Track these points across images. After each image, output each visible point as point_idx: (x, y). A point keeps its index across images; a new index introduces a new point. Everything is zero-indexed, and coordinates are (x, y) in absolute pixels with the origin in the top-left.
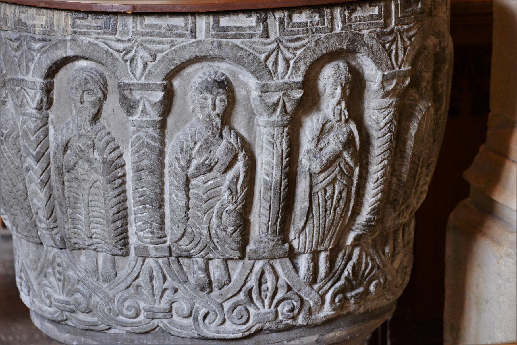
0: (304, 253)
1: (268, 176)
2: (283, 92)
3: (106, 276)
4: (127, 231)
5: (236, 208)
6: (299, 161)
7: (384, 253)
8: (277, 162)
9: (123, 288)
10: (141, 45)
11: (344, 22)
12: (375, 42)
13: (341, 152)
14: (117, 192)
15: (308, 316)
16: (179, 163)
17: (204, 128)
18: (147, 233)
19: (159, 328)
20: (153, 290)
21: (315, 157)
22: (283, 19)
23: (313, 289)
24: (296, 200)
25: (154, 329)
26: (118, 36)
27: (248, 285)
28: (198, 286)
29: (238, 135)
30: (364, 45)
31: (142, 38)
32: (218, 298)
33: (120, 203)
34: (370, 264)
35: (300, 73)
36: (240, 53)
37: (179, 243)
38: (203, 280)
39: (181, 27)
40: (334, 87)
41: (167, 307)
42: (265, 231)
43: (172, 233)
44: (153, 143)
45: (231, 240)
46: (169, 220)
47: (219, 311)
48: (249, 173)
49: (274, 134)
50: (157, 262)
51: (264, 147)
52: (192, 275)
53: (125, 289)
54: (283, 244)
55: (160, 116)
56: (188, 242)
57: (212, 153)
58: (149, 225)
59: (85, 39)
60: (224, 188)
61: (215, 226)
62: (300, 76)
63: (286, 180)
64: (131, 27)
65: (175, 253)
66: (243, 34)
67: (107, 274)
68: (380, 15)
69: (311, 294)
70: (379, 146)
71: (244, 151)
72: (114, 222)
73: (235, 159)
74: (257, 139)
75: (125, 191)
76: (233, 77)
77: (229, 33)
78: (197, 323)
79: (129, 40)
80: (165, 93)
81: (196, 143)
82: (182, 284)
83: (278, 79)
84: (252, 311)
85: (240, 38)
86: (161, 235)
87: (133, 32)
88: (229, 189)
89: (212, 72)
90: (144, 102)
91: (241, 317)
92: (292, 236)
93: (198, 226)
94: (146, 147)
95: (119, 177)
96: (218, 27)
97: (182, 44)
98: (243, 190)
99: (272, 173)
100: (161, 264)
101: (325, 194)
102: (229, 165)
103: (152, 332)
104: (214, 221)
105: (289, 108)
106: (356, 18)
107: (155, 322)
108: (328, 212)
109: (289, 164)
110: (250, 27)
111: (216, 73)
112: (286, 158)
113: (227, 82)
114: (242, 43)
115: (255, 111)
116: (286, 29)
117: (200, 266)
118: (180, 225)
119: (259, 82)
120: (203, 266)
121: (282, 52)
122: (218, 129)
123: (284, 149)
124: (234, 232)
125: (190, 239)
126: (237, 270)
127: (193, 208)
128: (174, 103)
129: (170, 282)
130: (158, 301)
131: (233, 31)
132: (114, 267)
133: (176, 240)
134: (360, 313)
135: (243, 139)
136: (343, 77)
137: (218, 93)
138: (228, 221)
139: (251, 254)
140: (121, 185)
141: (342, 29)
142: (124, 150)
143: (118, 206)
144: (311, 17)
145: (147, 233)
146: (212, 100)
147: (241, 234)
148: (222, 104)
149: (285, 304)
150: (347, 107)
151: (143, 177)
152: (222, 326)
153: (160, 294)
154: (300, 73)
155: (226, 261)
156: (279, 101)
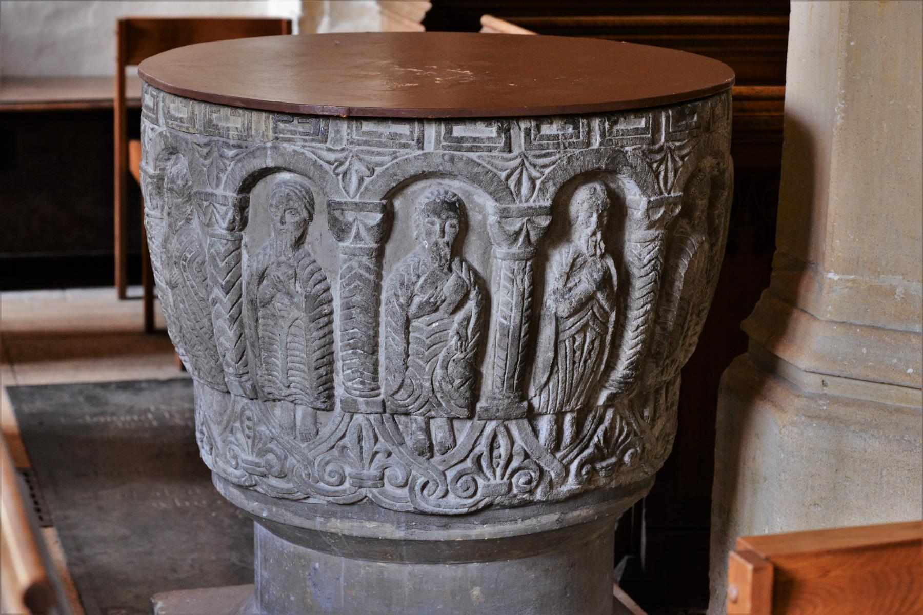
0: (546, 413)
4: (332, 380)
7: (642, 417)
10: (357, 156)
11: (603, 135)
12: (639, 161)
13: (595, 292)
14: (321, 332)
16: (398, 300)
18: (356, 383)
21: (563, 298)
22: (530, 130)
23: (555, 457)
25: (362, 500)
26: (328, 145)
27: (477, 450)
29: (470, 268)
30: (627, 164)
32: (440, 465)
33: (325, 346)
34: (625, 430)
35: (548, 196)
37: (395, 396)
40: (588, 214)
42: (499, 385)
44: (367, 275)
50: (368, 420)
55: (376, 243)
56: (406, 396)
57: (439, 289)
59: (288, 147)
60: (451, 332)
61: (439, 378)
64: (345, 134)
68: (646, 129)
70: (641, 287)
72: (316, 369)
73: (466, 297)
75: (331, 332)
79: (343, 150)
81: (419, 277)
83: (521, 202)
84: (481, 482)
89: (442, 192)
90: (358, 226)
92: (532, 392)
95: (325, 315)
98: (474, 336)
100: (373, 422)
101: (574, 343)
104: (439, 371)
105: (533, 238)
106: (618, 131)
107: (363, 491)
108: (577, 365)
110: (490, 139)
111: (446, 193)
113: (460, 204)
114: (479, 157)
115: (492, 241)
122: (447, 261)
126: (464, 431)
129: (382, 444)
130: (367, 466)
132: (316, 423)
134: (611, 489)
135: (476, 273)
136: (600, 202)
137: (447, 218)
140: (327, 325)
141: (601, 144)
144: (563, 128)
147: (470, 389)
149: (520, 475)
150: (604, 238)
154: (548, 196)
155: (451, 420)
156: (521, 230)
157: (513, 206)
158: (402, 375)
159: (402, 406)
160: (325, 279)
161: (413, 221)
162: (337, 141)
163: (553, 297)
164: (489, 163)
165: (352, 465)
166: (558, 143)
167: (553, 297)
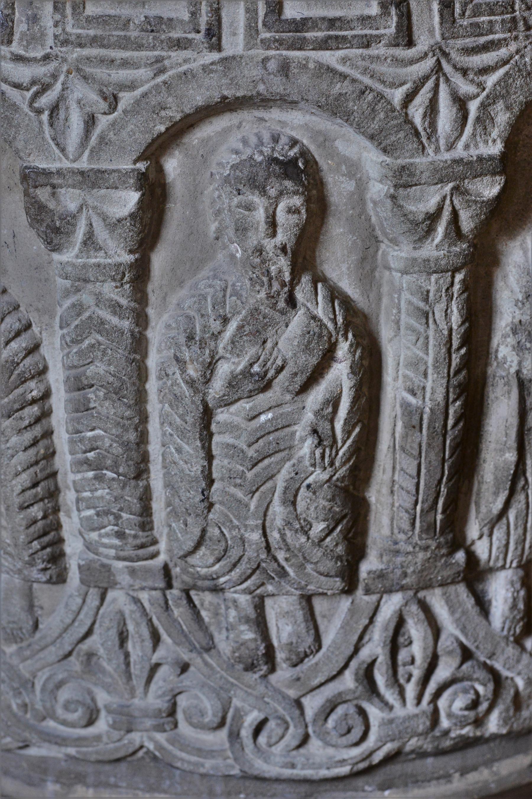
0: (503, 567)
1: (414, 394)
2: (451, 185)
3: (12, 629)
4: (58, 526)
5: (331, 477)
6: (493, 351)
8: (436, 361)
9: (53, 658)
10: (78, 70)
14: (28, 436)
15: (511, 712)
16: (183, 371)
17: (248, 282)
18: (107, 535)
19: (144, 750)
20: (128, 664)
23: (523, 649)
24: (484, 446)
25: (134, 753)
26: (16, 48)
27: (365, 654)
28: (240, 660)
29: (335, 294)
31: (78, 52)
32: (289, 687)
33: (37, 463)
35: (495, 134)
36: (337, 88)
37: (189, 559)
38: (252, 646)
39: (181, 22)
41: (163, 704)
42: (406, 526)
43: (171, 536)
44: (115, 320)
45: (320, 554)
46: (163, 505)
47: (292, 719)
48: (365, 389)
49: (428, 292)
50: (137, 601)
51: (402, 323)
52: (224, 633)
53: (59, 661)
54: (452, 552)
55: (131, 252)
56: (211, 560)
57: (269, 345)
58: (111, 518)
60: (300, 430)
61: (279, 522)
62: (494, 141)
63: (458, 403)
64: (51, 23)
65: (179, 580)
66: (344, 38)
67: (15, 626)
69: (518, 661)
71: (350, 335)
72: (23, 508)
73: (328, 357)
74: (385, 301)
75: (48, 434)
76: (319, 146)
77: (308, 35)
78: (237, 746)
79: (46, 58)
80: (143, 195)
81: (225, 321)
82: (200, 653)
83: (437, 150)
84: (374, 713)
85: (338, 48)
86: (144, 540)
87: (56, 37)
88: (315, 431)
89: (266, 137)
90: (89, 219)
91: (349, 731)
92: (473, 530)
93: (236, 522)
94: (99, 332)
95: (34, 401)
96: (279, 20)
97: (185, 67)
98: (349, 433)
99: (424, 388)
100: (147, 605)
102: (313, 372)
103: (129, 759)
104: (278, 510)
105: (467, 224)
107: (136, 737)
109: (467, 363)
110: (365, 20)
111: (275, 139)
112: (459, 349)
113: (306, 163)
114: (344, 60)
115: (378, 233)
116: (460, 22)
117: (243, 614)
118: (190, 520)
119: (388, 160)
120: (251, 613)
121: (447, 80)
122: (283, 284)
123: (455, 327)
124: (327, 535)
125: (216, 552)
126: (336, 617)
127: (222, 479)
128: (168, 215)
130: (140, 690)
131: (320, 29)
132: (31, 607)
133: (181, 553)
135: (347, 304)
137: (281, 193)
138: (312, 509)
139: (370, 582)
140: (38, 420)
142: (44, 334)
143: (32, 470)
145: (107, 535)
146: (266, 210)
147: (345, 538)
148: (294, 219)
149: (455, 694)
151: (92, 405)
152: (302, 751)
153: (145, 675)
154: (495, 134)
155: (307, 600)
156: (440, 209)
157: (420, 161)
158: (200, 520)
159: (205, 578)
160: (28, 326)
161: (207, 202)
162: (34, 39)
163: (511, 340)
164: (365, 71)
165: (108, 688)
166: (514, 20)
167: (511, 340)
